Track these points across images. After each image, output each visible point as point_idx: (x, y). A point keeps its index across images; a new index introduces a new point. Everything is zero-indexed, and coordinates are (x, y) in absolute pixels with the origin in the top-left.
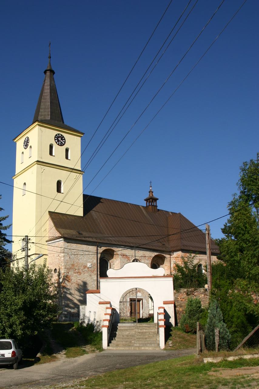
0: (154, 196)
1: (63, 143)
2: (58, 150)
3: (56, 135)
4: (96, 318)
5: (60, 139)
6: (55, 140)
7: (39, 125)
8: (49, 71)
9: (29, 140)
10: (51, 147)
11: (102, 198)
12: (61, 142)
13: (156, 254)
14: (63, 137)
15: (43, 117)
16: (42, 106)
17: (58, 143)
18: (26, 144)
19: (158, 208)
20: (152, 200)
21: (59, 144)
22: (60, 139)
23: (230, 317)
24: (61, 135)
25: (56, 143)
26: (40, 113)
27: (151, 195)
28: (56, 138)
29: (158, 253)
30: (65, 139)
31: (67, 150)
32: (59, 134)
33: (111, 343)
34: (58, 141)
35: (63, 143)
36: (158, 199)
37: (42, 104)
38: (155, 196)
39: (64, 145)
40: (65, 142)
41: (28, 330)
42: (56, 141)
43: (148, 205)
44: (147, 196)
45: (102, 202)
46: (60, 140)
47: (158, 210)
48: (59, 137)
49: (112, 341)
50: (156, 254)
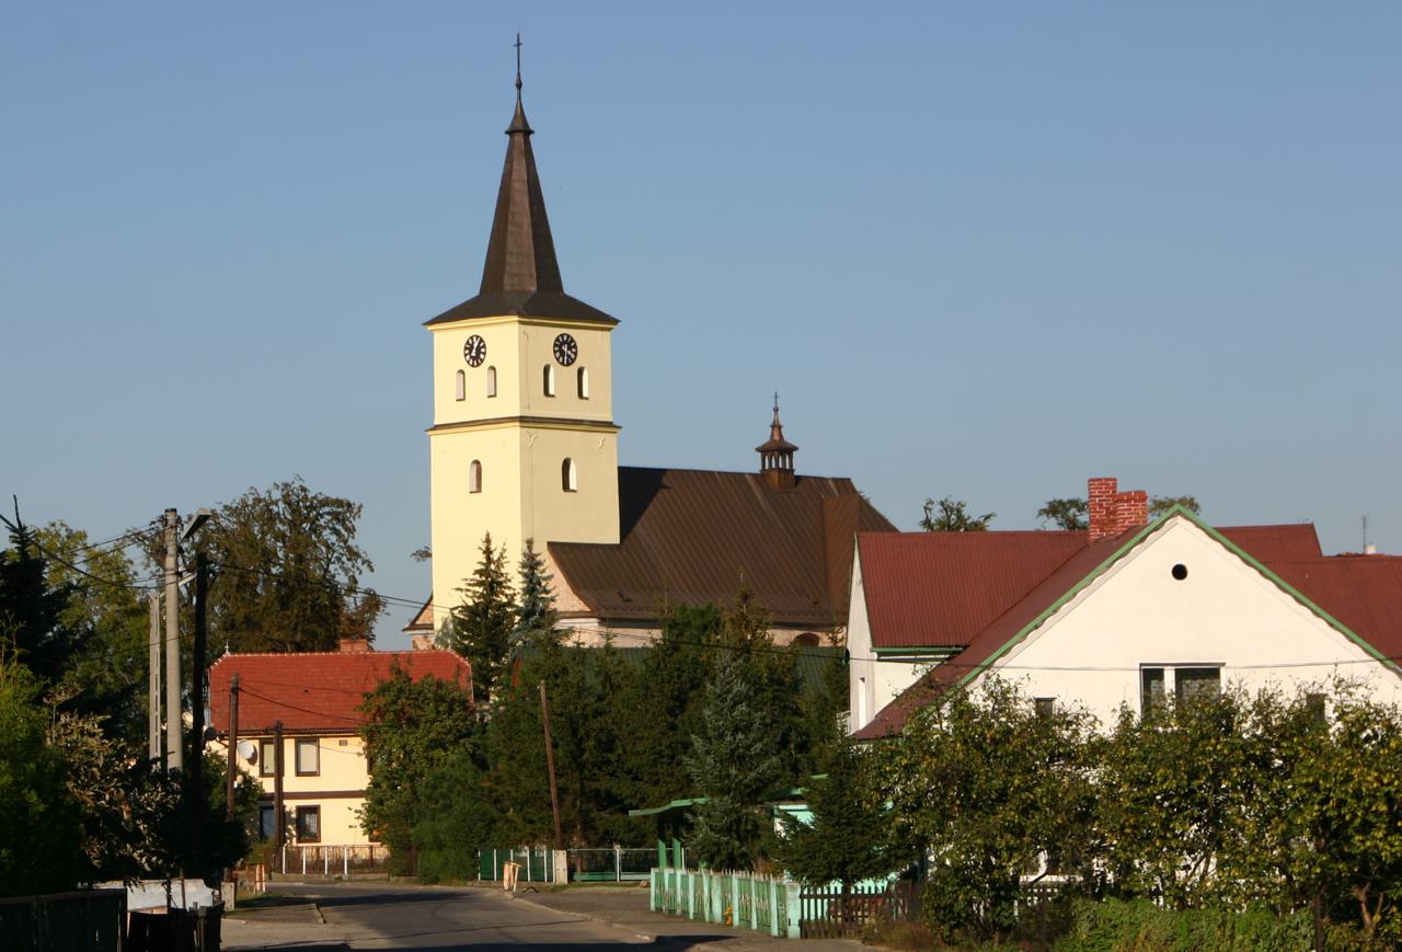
0: (785, 439)
1: (573, 356)
2: (561, 377)
3: (557, 339)
4: (356, 751)
5: (565, 348)
6: (555, 352)
7: (521, 322)
8: (521, 134)
9: (484, 346)
10: (546, 370)
11: (662, 472)
12: (569, 356)
13: (798, 633)
14: (572, 340)
15: (516, 280)
16: (511, 247)
17: (561, 360)
18: (473, 354)
19: (796, 473)
20: (778, 448)
21: (563, 364)
22: (565, 348)
23: (423, 799)
24: (568, 336)
25: (558, 359)
26: (508, 268)
27: (777, 438)
28: (557, 349)
29: (801, 630)
30: (575, 347)
31: (580, 372)
32: (562, 335)
33: (1307, 532)
34: (562, 354)
35: (573, 356)
36: (796, 449)
37: (510, 239)
38: (789, 437)
39: (573, 361)
40: (576, 354)
41: (153, 831)
42: (558, 354)
43: (767, 467)
44: (764, 437)
45: (665, 487)
46: (565, 350)
47: (799, 478)
48: (564, 343)
49: (1329, 548)
50: (798, 633)
